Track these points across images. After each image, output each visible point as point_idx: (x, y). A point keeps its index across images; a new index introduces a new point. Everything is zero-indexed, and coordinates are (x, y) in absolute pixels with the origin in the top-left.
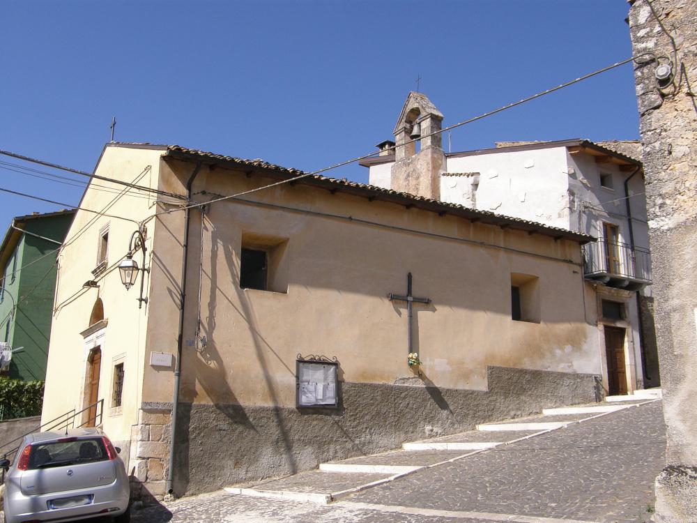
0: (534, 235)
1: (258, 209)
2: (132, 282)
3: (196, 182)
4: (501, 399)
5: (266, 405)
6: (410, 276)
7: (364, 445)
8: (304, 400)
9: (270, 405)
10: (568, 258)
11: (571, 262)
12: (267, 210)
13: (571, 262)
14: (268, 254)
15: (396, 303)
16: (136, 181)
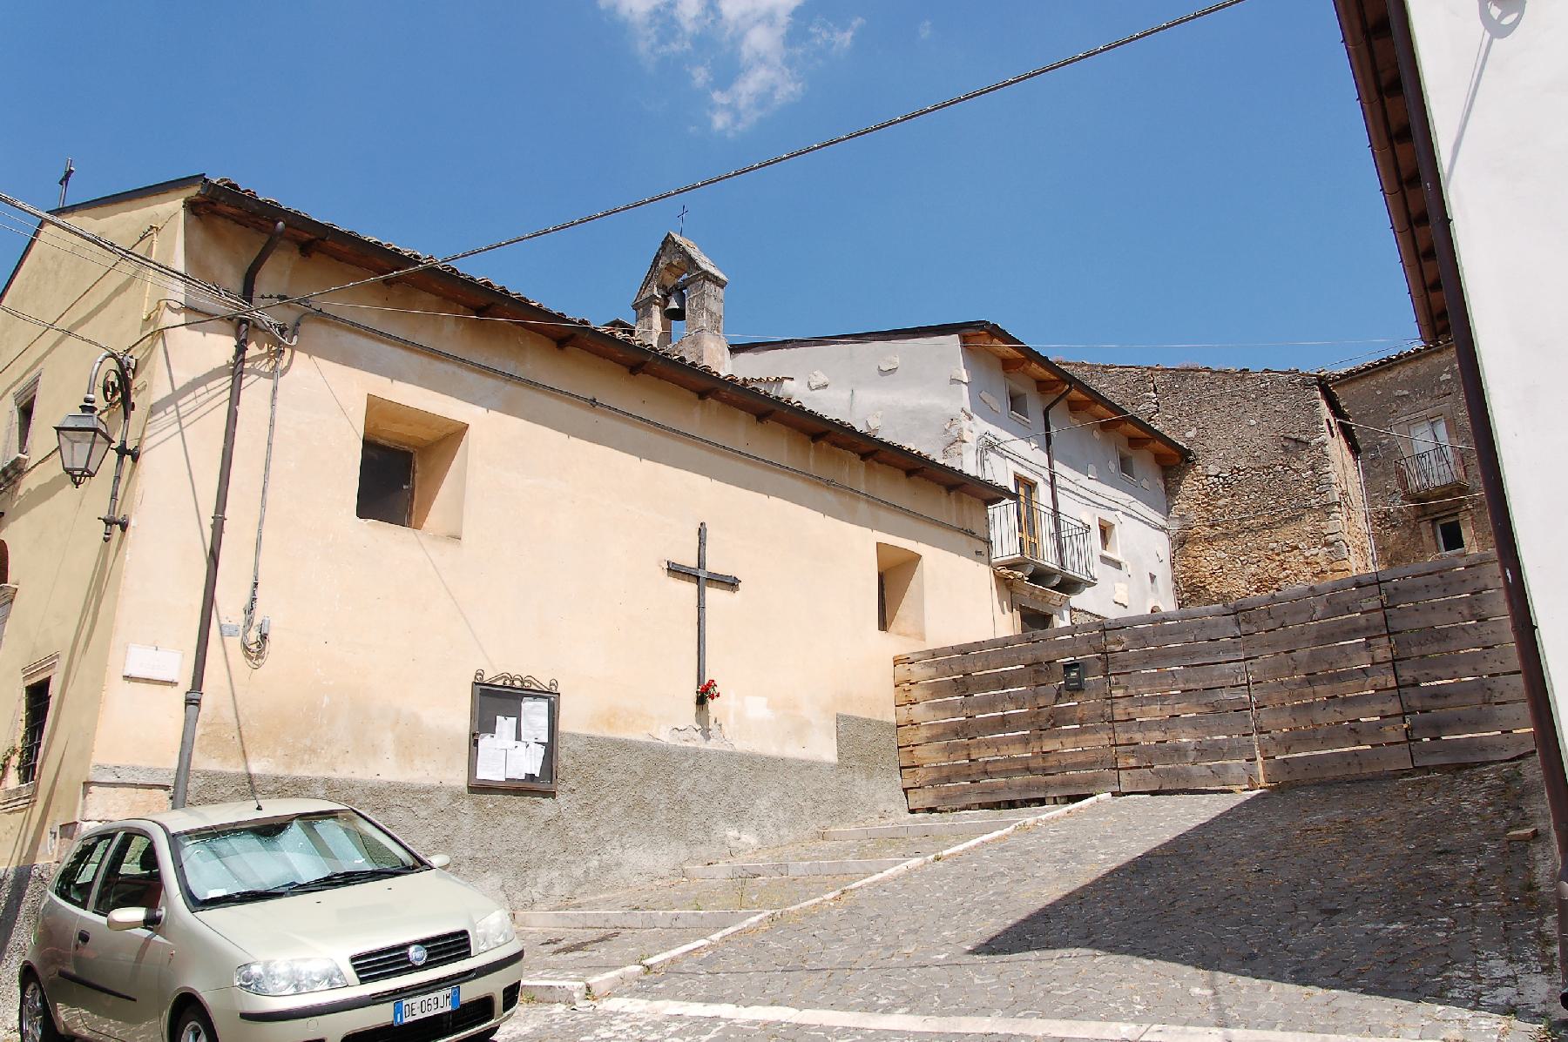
0: (915, 478)
1: (404, 353)
2: (92, 468)
3: (267, 282)
4: (860, 780)
5: (232, 770)
6: (702, 532)
7: (608, 869)
8: (482, 775)
9: (241, 769)
10: (967, 527)
11: (972, 534)
12: (425, 360)
13: (972, 534)
14: (416, 458)
15: (959, 500)
16: (116, 279)
